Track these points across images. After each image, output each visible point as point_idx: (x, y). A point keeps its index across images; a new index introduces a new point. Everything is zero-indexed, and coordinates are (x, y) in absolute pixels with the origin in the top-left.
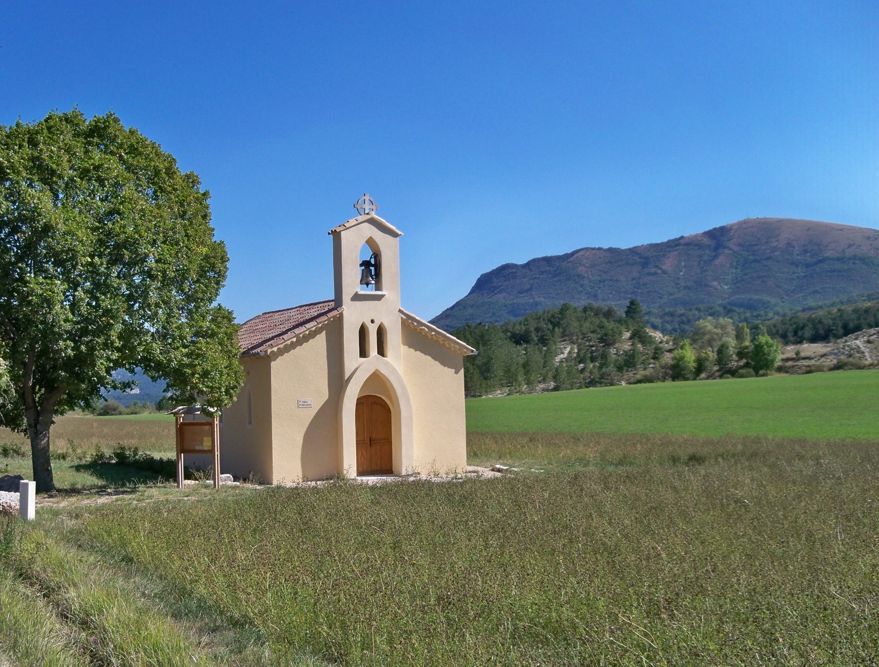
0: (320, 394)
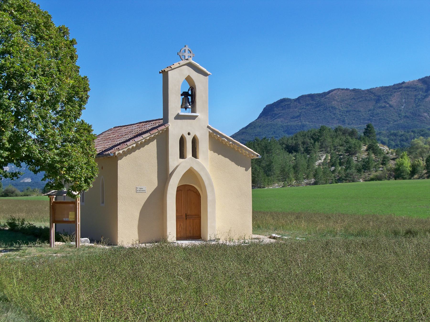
0: (151, 183)
